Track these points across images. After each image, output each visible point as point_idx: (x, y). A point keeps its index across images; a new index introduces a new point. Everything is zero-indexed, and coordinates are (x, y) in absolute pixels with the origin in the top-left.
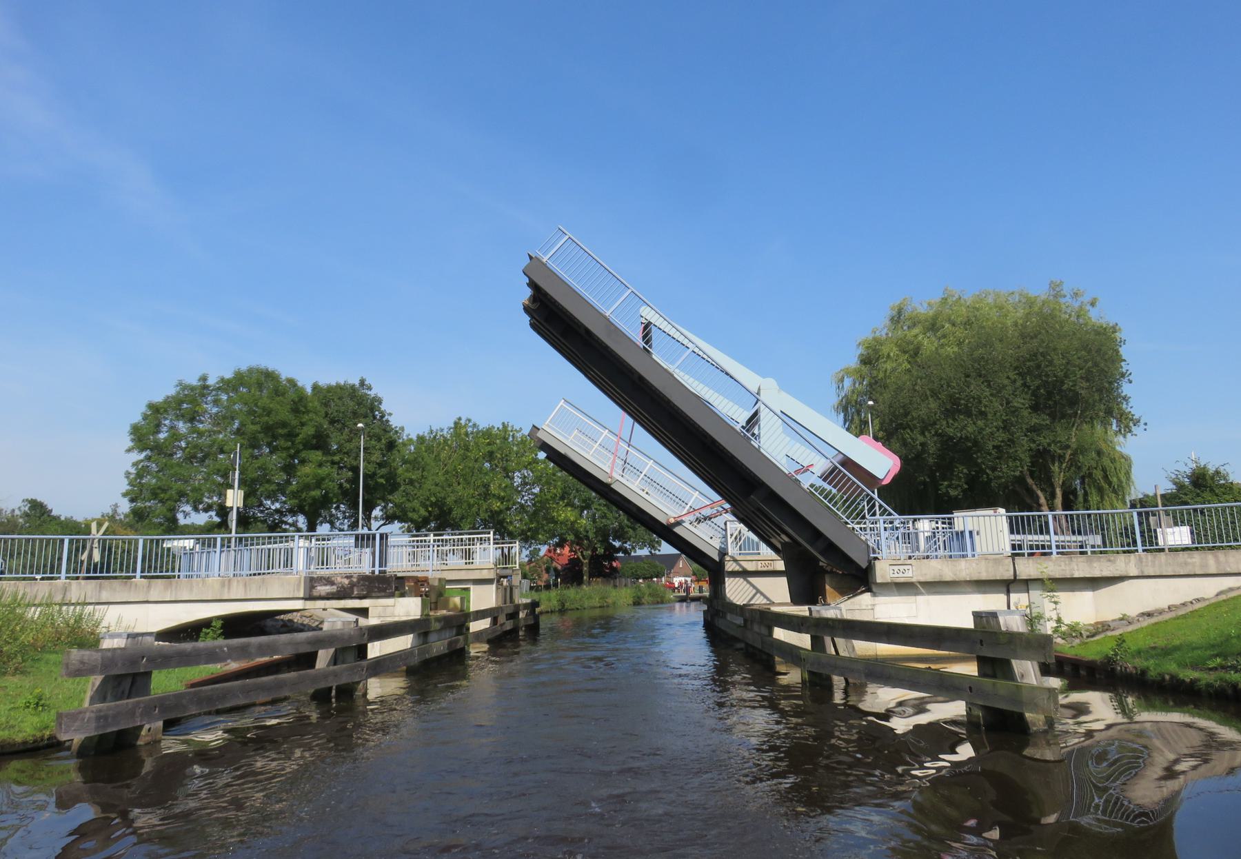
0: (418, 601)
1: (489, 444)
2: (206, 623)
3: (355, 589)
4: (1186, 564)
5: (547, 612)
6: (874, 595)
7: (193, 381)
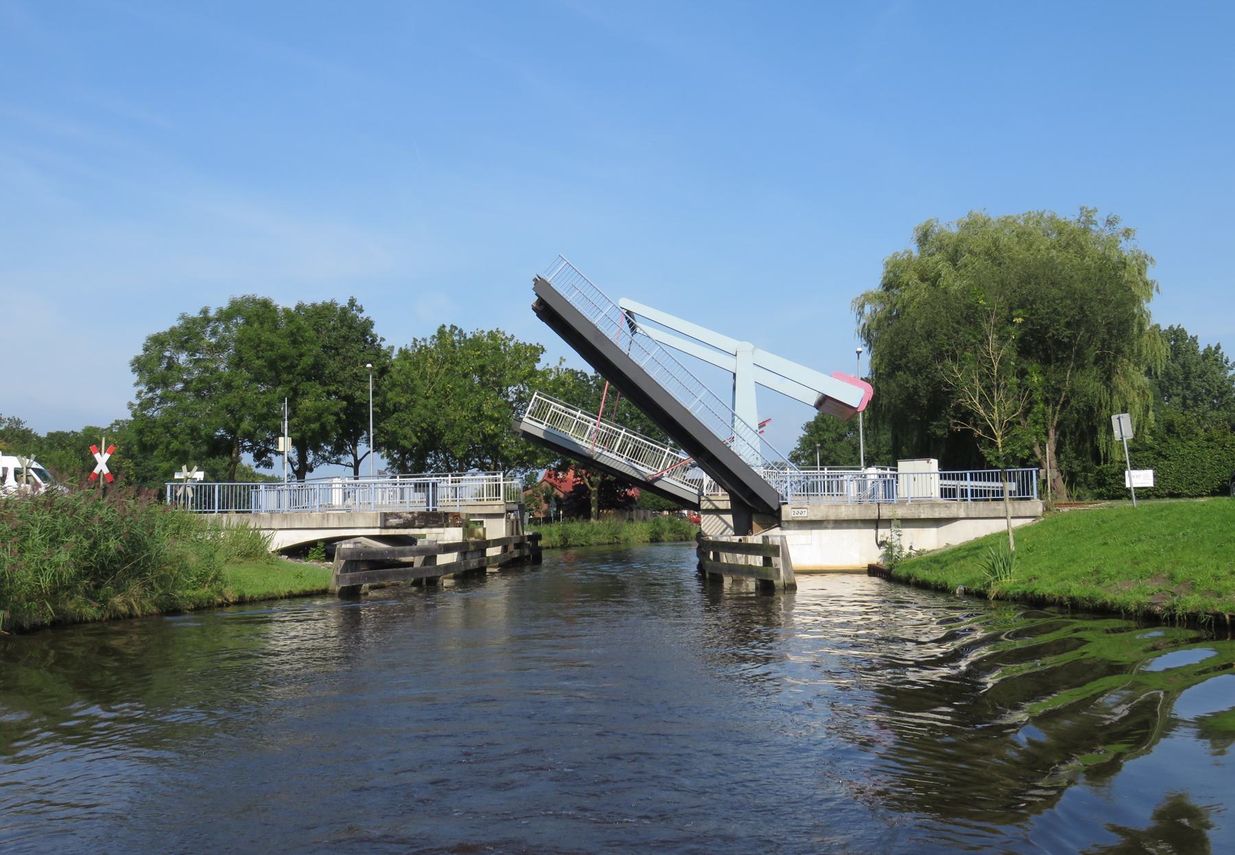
0: (460, 530)
1: (479, 357)
2: (313, 544)
3: (416, 521)
4: (995, 509)
5: (548, 548)
6: (782, 529)
7: (195, 313)
